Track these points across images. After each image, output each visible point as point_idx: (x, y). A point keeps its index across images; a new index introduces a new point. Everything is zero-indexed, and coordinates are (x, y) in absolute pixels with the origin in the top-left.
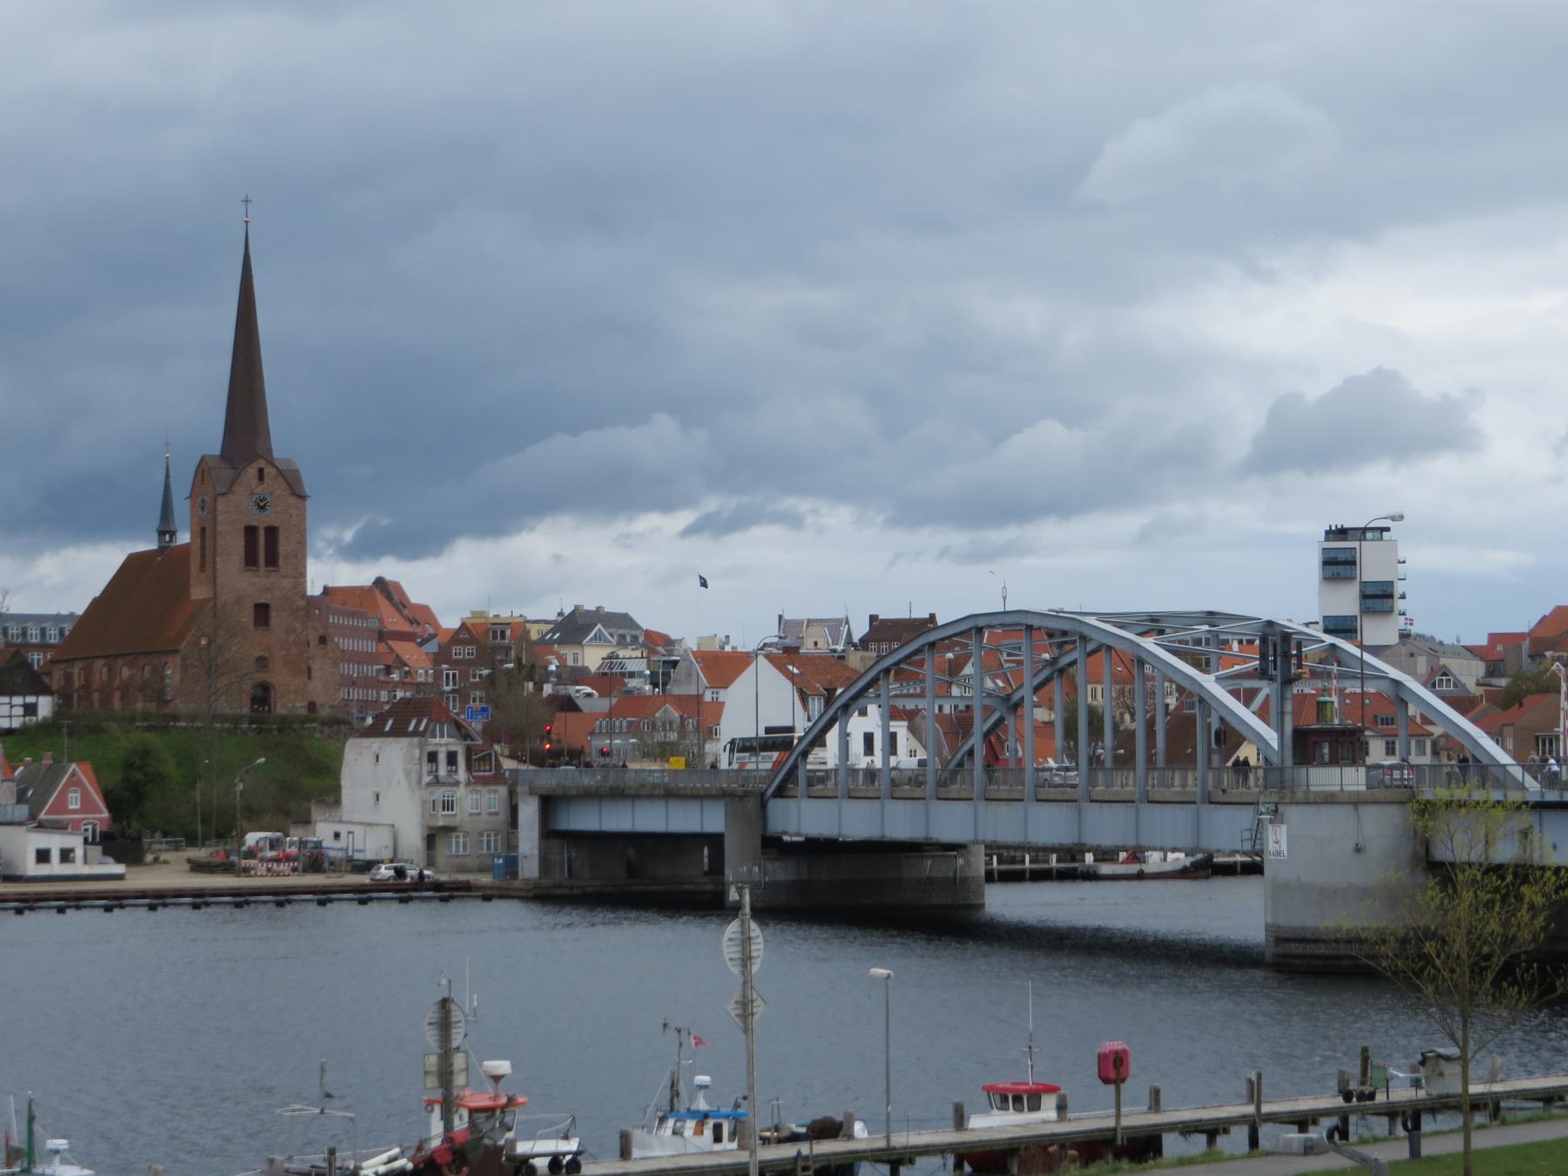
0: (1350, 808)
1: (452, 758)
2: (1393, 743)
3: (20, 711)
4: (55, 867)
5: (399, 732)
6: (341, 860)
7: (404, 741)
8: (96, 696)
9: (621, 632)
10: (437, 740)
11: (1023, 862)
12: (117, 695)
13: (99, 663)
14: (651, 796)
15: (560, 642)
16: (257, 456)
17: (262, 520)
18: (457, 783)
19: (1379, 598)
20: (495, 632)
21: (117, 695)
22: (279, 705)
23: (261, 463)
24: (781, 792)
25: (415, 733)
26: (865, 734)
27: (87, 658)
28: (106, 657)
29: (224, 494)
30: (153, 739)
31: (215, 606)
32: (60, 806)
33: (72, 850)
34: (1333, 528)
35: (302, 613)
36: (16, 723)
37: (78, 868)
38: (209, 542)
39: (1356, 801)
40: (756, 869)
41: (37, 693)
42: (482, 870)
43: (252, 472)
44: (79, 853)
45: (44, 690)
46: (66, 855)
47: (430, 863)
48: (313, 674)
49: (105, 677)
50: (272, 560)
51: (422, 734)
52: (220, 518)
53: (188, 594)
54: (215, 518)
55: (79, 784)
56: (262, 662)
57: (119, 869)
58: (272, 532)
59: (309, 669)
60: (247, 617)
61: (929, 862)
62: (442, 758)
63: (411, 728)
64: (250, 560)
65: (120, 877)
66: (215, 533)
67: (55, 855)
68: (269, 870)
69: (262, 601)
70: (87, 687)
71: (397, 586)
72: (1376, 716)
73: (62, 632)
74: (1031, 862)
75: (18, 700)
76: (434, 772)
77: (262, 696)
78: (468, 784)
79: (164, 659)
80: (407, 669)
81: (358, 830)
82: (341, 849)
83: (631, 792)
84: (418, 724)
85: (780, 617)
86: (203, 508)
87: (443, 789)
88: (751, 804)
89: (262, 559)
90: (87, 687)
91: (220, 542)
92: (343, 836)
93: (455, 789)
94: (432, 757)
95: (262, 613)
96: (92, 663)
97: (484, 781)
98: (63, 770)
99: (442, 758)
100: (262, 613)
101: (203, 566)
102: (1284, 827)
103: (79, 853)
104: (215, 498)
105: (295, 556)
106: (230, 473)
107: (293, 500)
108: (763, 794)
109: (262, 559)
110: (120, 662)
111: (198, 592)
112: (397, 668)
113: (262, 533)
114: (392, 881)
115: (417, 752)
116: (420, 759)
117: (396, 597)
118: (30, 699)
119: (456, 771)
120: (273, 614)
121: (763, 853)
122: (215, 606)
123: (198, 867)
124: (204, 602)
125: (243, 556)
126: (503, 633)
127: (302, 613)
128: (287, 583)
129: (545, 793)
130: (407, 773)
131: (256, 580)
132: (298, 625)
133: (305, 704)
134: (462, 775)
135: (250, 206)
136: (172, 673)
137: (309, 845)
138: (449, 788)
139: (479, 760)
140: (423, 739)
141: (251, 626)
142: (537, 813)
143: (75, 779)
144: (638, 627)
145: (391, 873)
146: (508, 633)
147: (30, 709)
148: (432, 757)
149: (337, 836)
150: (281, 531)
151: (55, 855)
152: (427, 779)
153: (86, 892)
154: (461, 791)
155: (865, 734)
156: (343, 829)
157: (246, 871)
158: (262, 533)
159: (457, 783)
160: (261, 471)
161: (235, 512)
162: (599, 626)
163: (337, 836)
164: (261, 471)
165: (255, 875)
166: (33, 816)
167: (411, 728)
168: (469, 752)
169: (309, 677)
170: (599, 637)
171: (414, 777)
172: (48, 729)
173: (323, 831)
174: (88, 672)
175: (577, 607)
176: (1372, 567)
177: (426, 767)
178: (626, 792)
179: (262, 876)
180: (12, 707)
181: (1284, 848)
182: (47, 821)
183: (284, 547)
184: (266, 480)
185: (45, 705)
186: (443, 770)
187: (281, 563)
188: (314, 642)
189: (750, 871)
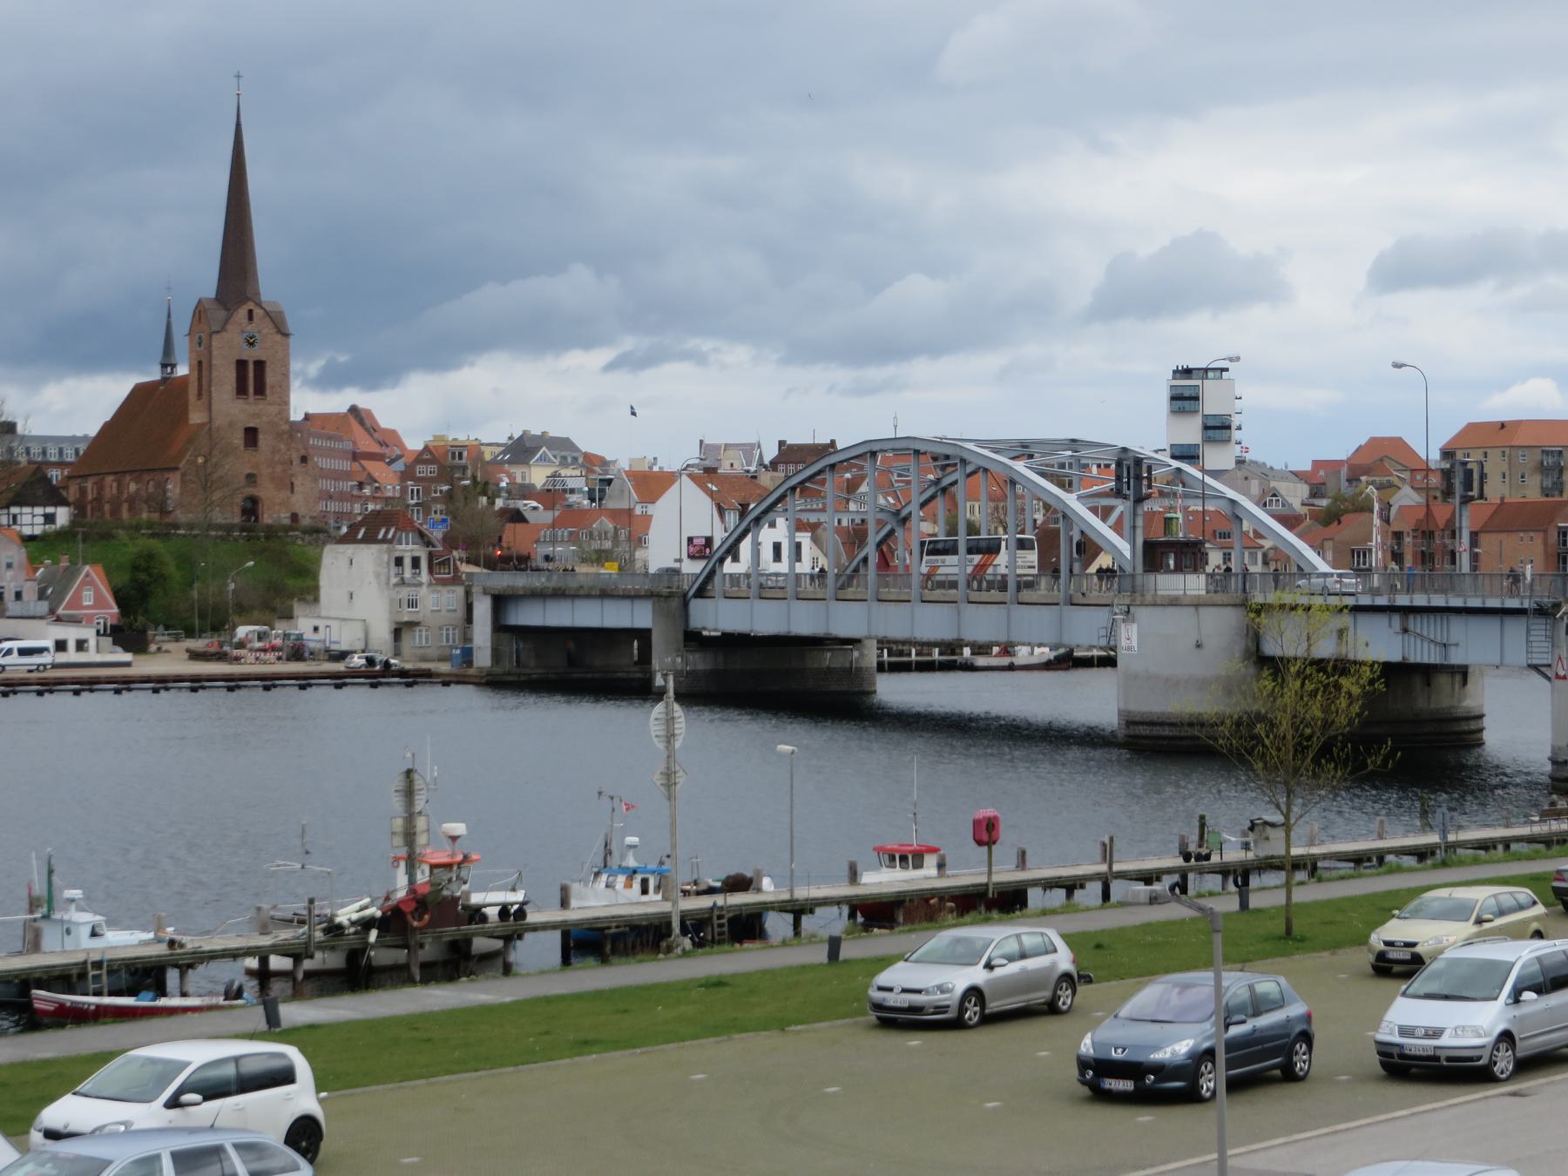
0: (1192, 609)
1: (416, 562)
2: (1230, 554)
3: (41, 520)
4: (71, 655)
5: (370, 539)
6: (320, 650)
7: (374, 548)
8: (107, 507)
9: (563, 453)
10: (403, 547)
11: (910, 655)
12: (125, 507)
13: (109, 479)
14: (588, 596)
15: (509, 462)
16: (246, 299)
17: (251, 355)
18: (420, 584)
19: (1218, 429)
20: (454, 454)
21: (125, 507)
22: (265, 516)
23: (251, 305)
24: (701, 593)
25: (384, 541)
26: (774, 543)
27: (99, 474)
28: (116, 473)
29: (218, 332)
30: (156, 545)
31: (210, 429)
32: (76, 603)
33: (85, 641)
34: (1180, 368)
35: (286, 436)
36: (38, 531)
37: (91, 656)
38: (205, 373)
39: (1197, 604)
40: (679, 660)
41: (56, 505)
42: (442, 659)
43: (242, 313)
44: (92, 643)
45: (63, 502)
46: (81, 645)
47: (397, 654)
48: (296, 489)
49: (114, 491)
50: (260, 390)
51: (390, 542)
52: (215, 353)
53: (187, 420)
54: (210, 353)
55: (92, 583)
56: (251, 478)
57: (127, 657)
58: (260, 365)
59: (292, 484)
60: (238, 439)
61: (829, 655)
62: (407, 562)
63: (380, 536)
64: (241, 390)
65: (127, 664)
66: (210, 366)
67: (71, 645)
68: (257, 659)
69: (251, 425)
70: (99, 499)
71: (369, 413)
72: (1215, 531)
73: (77, 451)
74: (917, 655)
75: (39, 510)
76: (400, 575)
77: (251, 508)
78: (430, 584)
79: (166, 475)
80: (377, 485)
81: (335, 625)
82: (320, 641)
83: (572, 593)
84: (387, 533)
85: (701, 442)
86: (200, 344)
87: (409, 589)
88: (675, 603)
89: (251, 390)
90: (99, 499)
91: (215, 374)
92: (321, 629)
93: (418, 589)
94: (399, 562)
95: (251, 435)
96: (103, 479)
97: (444, 583)
98: (78, 571)
99: (407, 562)
100: (251, 435)
101: (200, 395)
102: (1135, 627)
103: (92, 643)
104: (211, 336)
105: (280, 386)
106: (222, 314)
107: (278, 337)
108: (685, 595)
109: (251, 390)
110: (128, 478)
111: (196, 417)
112: (369, 484)
113: (251, 367)
114: (363, 669)
115: (385, 557)
116: (388, 563)
117: (368, 423)
118: (50, 510)
119: (420, 573)
120: (261, 436)
121: (685, 646)
122: (210, 429)
123: (195, 656)
124: (201, 426)
125: (235, 385)
126: (460, 455)
127: (286, 436)
128: (273, 409)
129: (497, 593)
130: (377, 575)
131: (246, 407)
132: (283, 446)
133: (288, 515)
134: (424, 576)
135: (241, 80)
136: (173, 487)
137: (292, 637)
138: (413, 589)
139: (439, 563)
140: (391, 546)
141: (242, 448)
142: (490, 610)
143: (88, 579)
144: (578, 450)
145: (363, 661)
146: (465, 454)
147: (50, 519)
148: (399, 562)
149: (316, 629)
150: (268, 364)
151: (71, 645)
152: (394, 580)
153: (98, 677)
154: (424, 591)
155: (774, 543)
156: (321, 624)
157: (237, 659)
158: (251, 367)
159: (420, 584)
160: (250, 312)
161: (228, 348)
162: (544, 449)
163: (316, 629)
164: (250, 312)
165: (245, 663)
166: (52, 611)
167: (380, 536)
168: (431, 556)
169: (292, 492)
170: (544, 459)
171: (383, 578)
172: (65, 535)
173: (303, 625)
174: (100, 487)
175: (525, 432)
176: (1213, 401)
177: (394, 570)
178: (567, 593)
179: (251, 664)
180: (34, 516)
181: (1135, 643)
182: (64, 615)
183: (270, 378)
184: (255, 320)
185: (63, 515)
186: (408, 572)
187: (268, 392)
188: (296, 461)
189: (674, 662)
